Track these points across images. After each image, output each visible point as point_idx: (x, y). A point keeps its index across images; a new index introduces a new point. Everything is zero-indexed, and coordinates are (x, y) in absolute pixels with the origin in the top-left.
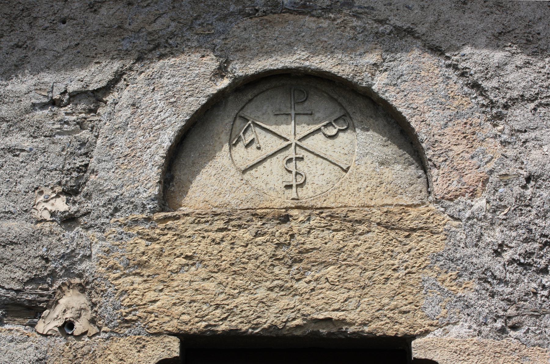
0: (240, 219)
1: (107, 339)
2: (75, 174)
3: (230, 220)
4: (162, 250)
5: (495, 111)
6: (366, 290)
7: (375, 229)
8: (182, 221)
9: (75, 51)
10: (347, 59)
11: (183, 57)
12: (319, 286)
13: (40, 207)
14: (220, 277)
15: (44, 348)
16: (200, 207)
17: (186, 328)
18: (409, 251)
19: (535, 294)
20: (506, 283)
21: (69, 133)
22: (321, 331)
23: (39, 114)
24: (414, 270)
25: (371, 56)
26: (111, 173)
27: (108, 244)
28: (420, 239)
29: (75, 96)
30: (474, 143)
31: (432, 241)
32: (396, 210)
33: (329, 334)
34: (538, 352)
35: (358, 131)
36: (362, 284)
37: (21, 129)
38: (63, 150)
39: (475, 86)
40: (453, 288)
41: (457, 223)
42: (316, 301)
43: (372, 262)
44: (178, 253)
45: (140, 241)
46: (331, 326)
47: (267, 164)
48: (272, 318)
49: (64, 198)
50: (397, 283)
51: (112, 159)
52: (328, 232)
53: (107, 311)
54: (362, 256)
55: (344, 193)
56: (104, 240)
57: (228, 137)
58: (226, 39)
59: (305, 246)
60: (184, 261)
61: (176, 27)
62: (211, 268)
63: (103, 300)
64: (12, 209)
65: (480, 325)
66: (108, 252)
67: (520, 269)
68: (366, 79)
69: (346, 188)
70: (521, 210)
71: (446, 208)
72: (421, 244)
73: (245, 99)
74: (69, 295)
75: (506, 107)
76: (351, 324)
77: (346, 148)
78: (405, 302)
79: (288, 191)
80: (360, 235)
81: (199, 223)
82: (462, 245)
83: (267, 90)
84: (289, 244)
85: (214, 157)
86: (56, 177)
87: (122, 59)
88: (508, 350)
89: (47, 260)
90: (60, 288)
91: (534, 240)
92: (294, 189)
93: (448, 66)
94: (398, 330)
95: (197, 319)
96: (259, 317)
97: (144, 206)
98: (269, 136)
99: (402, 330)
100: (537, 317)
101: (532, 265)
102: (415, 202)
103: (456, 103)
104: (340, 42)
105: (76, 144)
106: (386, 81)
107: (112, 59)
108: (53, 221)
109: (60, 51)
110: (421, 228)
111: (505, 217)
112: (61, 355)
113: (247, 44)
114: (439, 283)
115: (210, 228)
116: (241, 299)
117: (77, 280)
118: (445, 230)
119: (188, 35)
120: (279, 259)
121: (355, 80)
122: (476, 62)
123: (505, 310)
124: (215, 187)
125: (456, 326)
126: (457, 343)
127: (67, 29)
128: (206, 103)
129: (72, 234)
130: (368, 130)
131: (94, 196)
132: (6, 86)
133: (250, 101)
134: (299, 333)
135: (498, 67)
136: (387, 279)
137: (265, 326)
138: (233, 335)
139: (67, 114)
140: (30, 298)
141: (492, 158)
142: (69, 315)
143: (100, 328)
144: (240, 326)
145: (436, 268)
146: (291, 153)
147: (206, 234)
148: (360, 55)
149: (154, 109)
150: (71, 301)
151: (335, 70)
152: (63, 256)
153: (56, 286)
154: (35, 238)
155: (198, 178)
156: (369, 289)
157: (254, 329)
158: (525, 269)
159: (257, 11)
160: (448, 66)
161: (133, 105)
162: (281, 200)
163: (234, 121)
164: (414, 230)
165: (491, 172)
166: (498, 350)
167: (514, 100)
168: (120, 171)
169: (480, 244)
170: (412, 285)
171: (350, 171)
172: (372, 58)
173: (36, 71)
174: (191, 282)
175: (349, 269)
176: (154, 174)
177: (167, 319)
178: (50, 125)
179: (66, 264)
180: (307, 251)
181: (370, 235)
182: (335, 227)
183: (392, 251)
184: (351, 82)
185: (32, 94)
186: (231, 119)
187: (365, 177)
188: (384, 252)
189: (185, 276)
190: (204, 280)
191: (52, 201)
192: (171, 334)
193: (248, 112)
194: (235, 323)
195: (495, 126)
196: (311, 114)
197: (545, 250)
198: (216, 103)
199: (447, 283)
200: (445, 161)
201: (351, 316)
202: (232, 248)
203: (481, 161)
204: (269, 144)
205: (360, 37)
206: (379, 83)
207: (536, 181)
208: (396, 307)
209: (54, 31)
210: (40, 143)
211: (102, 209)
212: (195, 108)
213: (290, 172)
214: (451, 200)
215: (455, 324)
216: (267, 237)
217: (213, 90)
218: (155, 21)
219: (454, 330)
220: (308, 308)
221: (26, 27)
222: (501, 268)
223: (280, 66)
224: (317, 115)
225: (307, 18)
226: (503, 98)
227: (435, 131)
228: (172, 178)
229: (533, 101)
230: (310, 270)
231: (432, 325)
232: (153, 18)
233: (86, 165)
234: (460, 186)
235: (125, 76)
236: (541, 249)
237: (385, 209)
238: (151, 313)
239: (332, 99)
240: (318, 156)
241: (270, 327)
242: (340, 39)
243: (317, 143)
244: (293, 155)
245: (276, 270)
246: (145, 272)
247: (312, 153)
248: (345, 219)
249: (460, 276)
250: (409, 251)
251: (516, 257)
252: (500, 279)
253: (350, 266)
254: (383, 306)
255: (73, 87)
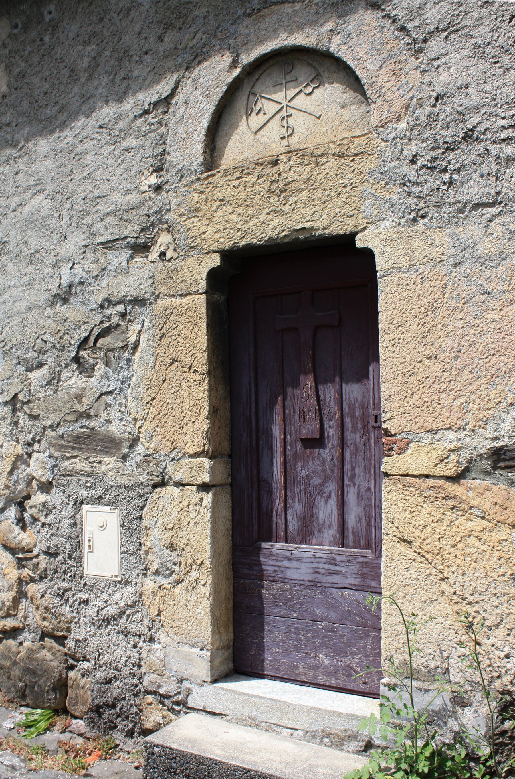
0: (248, 168)
1: (183, 259)
2: (159, 158)
3: (243, 170)
4: (207, 198)
5: (417, 46)
6: (326, 205)
7: (331, 159)
8: (217, 176)
9: (153, 73)
10: (313, 31)
11: (211, 59)
12: (297, 207)
13: (143, 183)
14: (239, 210)
15: (153, 270)
16: (232, 164)
17: (222, 247)
18: (353, 171)
19: (438, 189)
20: (418, 184)
21: (155, 131)
22: (300, 237)
23: (139, 121)
24: (357, 184)
25: (328, 24)
26: (177, 153)
27: (178, 200)
28: (360, 161)
29: (156, 104)
30: (401, 77)
31: (369, 161)
32: (344, 142)
33: (305, 238)
34: (438, 233)
35: (326, 85)
36: (323, 200)
37: (131, 135)
38: (152, 143)
39: (403, 29)
40: (383, 194)
41: (386, 144)
42: (295, 218)
43: (329, 184)
44: (215, 199)
45: (195, 194)
46: (306, 233)
47: (269, 124)
48: (270, 233)
49: (155, 174)
50: (345, 196)
51: (177, 143)
52: (301, 167)
53: (182, 242)
54: (323, 180)
55: (317, 135)
56: (176, 198)
57: (245, 110)
58: (236, 38)
59: (287, 180)
60: (219, 203)
61: (206, 38)
62: (234, 205)
63: (179, 236)
64: (130, 188)
65: (400, 218)
66: (179, 205)
67: (428, 171)
68: (325, 44)
69: (318, 131)
70: (431, 125)
71: (379, 134)
72: (361, 165)
73: (254, 79)
74: (162, 235)
75: (425, 41)
76: (317, 230)
77: (319, 101)
78: (351, 209)
79: (284, 141)
80: (322, 165)
81: (226, 176)
82: (389, 160)
83: (267, 69)
84: (278, 180)
85: (237, 127)
86: (150, 161)
87: (178, 71)
88: (417, 234)
89: (149, 216)
90: (157, 232)
91: (439, 148)
92: (286, 139)
93: (384, 17)
94: (346, 230)
95: (228, 240)
96: (262, 233)
97: (196, 171)
98: (270, 103)
99: (349, 229)
100: (439, 206)
101: (436, 168)
102: (364, 133)
103: (389, 47)
104: (307, 19)
105: (158, 137)
106: (339, 42)
107: (173, 73)
108: (150, 191)
109: (146, 75)
110: (362, 153)
111: (418, 133)
112: (161, 273)
113: (249, 38)
114: (373, 192)
115: (232, 178)
116: (252, 223)
117: (165, 226)
118: (378, 151)
119: (214, 42)
120: (272, 192)
121: (318, 47)
122: (403, 8)
123: (417, 205)
124: (239, 148)
125: (385, 221)
126: (384, 233)
127: (148, 58)
128: (227, 90)
129: (160, 197)
130: (332, 83)
131: (170, 170)
132: (120, 108)
133: (257, 80)
134: (287, 240)
135: (420, 8)
136: (339, 194)
137: (266, 239)
138: (249, 247)
139: (153, 118)
140: (143, 241)
141: (413, 86)
142: (162, 248)
143: (179, 254)
144: (252, 241)
145: (371, 181)
146: (283, 113)
147: (230, 183)
148: (321, 25)
149: (197, 102)
150: (164, 239)
151: (304, 43)
152: (156, 213)
153: (155, 231)
154: (142, 203)
155: (229, 144)
156: (328, 203)
157: (260, 241)
158: (432, 171)
159: (254, 10)
160: (384, 17)
161: (186, 102)
162: (278, 148)
163: (249, 98)
164: (356, 155)
165: (412, 98)
166: (411, 234)
167: (431, 34)
168: (182, 150)
169: (401, 157)
170: (355, 196)
171: (321, 118)
172: (330, 25)
173: (135, 93)
174: (223, 216)
175: (315, 191)
176: (199, 147)
177: (212, 242)
178: (145, 128)
179: (159, 216)
180: (289, 183)
181: (328, 164)
182: (306, 162)
183: (342, 173)
184: (316, 49)
185: (134, 110)
186: (246, 97)
187: (331, 120)
188: (337, 175)
189: (220, 213)
190: (230, 214)
191: (149, 178)
192: (215, 252)
193: (257, 89)
194: (251, 240)
195: (417, 59)
196: (296, 80)
197: (447, 154)
198: (234, 89)
199: (379, 191)
200: (380, 96)
201: (316, 225)
202: (245, 189)
203: (405, 91)
204: (270, 108)
205: (321, 10)
206: (335, 46)
207: (443, 99)
208: (345, 214)
209: (142, 62)
210: (141, 141)
211: (174, 178)
212: (220, 96)
213: (284, 127)
214: (383, 127)
215: (384, 219)
216: (265, 178)
217: (230, 80)
218: (194, 38)
219: (383, 225)
220: (291, 222)
221: (127, 63)
222: (415, 173)
223: (269, 49)
224: (300, 79)
225: (286, 6)
226: (423, 34)
227: (373, 74)
228: (215, 147)
229: (446, 31)
230: (291, 196)
231: (368, 223)
232: (192, 35)
233: (164, 151)
234: (389, 115)
235: (181, 83)
236: (444, 153)
237: (338, 143)
238: (203, 240)
239: (310, 65)
240: (301, 111)
241: (269, 239)
242: (307, 16)
243: (301, 101)
244: (284, 114)
245: (271, 200)
246: (199, 214)
247: (297, 109)
248: (312, 155)
249: (388, 184)
250: (353, 171)
251: (425, 163)
252: (413, 182)
253: (315, 189)
254: (337, 214)
255: (154, 98)
